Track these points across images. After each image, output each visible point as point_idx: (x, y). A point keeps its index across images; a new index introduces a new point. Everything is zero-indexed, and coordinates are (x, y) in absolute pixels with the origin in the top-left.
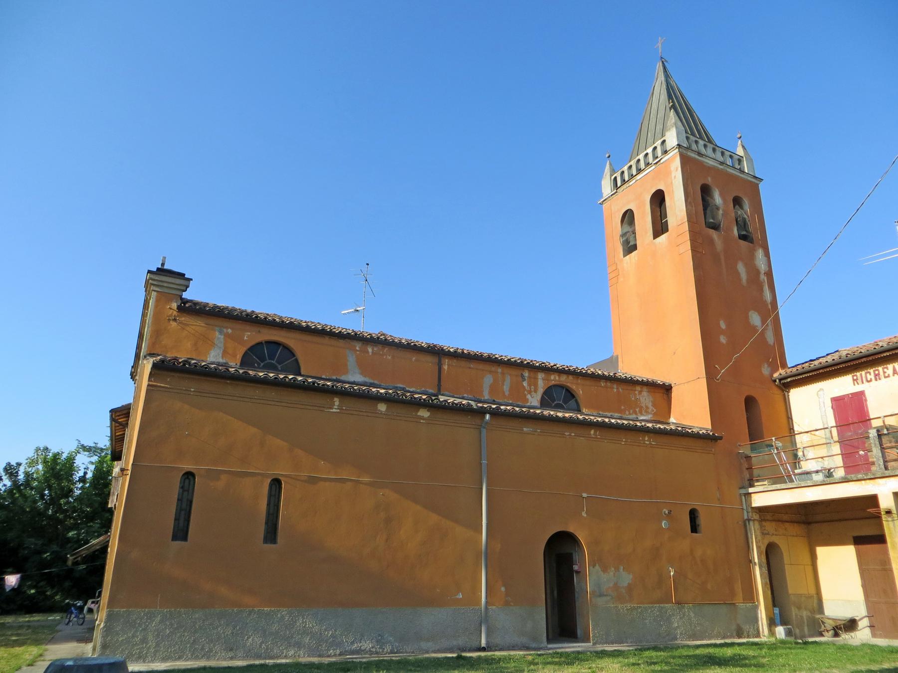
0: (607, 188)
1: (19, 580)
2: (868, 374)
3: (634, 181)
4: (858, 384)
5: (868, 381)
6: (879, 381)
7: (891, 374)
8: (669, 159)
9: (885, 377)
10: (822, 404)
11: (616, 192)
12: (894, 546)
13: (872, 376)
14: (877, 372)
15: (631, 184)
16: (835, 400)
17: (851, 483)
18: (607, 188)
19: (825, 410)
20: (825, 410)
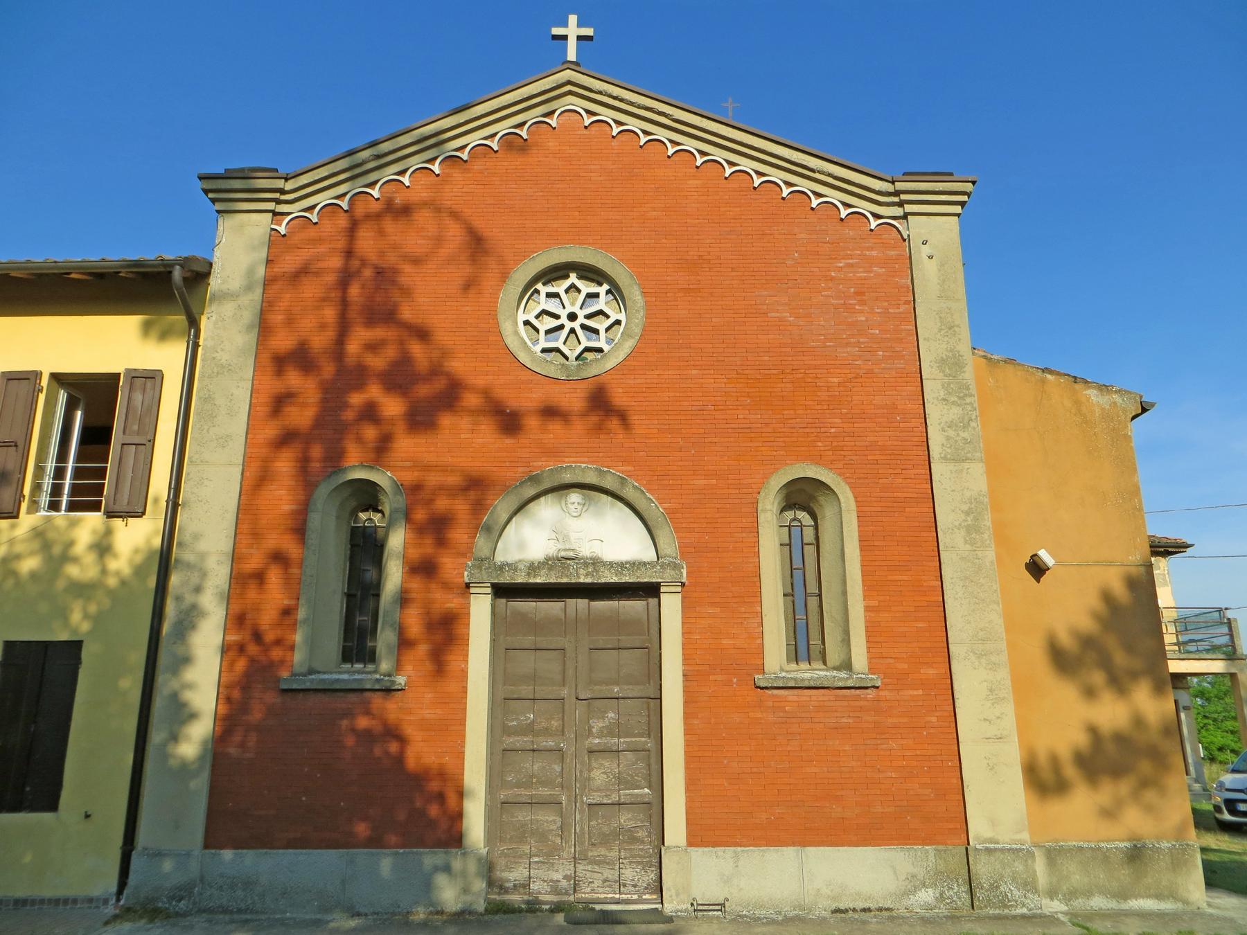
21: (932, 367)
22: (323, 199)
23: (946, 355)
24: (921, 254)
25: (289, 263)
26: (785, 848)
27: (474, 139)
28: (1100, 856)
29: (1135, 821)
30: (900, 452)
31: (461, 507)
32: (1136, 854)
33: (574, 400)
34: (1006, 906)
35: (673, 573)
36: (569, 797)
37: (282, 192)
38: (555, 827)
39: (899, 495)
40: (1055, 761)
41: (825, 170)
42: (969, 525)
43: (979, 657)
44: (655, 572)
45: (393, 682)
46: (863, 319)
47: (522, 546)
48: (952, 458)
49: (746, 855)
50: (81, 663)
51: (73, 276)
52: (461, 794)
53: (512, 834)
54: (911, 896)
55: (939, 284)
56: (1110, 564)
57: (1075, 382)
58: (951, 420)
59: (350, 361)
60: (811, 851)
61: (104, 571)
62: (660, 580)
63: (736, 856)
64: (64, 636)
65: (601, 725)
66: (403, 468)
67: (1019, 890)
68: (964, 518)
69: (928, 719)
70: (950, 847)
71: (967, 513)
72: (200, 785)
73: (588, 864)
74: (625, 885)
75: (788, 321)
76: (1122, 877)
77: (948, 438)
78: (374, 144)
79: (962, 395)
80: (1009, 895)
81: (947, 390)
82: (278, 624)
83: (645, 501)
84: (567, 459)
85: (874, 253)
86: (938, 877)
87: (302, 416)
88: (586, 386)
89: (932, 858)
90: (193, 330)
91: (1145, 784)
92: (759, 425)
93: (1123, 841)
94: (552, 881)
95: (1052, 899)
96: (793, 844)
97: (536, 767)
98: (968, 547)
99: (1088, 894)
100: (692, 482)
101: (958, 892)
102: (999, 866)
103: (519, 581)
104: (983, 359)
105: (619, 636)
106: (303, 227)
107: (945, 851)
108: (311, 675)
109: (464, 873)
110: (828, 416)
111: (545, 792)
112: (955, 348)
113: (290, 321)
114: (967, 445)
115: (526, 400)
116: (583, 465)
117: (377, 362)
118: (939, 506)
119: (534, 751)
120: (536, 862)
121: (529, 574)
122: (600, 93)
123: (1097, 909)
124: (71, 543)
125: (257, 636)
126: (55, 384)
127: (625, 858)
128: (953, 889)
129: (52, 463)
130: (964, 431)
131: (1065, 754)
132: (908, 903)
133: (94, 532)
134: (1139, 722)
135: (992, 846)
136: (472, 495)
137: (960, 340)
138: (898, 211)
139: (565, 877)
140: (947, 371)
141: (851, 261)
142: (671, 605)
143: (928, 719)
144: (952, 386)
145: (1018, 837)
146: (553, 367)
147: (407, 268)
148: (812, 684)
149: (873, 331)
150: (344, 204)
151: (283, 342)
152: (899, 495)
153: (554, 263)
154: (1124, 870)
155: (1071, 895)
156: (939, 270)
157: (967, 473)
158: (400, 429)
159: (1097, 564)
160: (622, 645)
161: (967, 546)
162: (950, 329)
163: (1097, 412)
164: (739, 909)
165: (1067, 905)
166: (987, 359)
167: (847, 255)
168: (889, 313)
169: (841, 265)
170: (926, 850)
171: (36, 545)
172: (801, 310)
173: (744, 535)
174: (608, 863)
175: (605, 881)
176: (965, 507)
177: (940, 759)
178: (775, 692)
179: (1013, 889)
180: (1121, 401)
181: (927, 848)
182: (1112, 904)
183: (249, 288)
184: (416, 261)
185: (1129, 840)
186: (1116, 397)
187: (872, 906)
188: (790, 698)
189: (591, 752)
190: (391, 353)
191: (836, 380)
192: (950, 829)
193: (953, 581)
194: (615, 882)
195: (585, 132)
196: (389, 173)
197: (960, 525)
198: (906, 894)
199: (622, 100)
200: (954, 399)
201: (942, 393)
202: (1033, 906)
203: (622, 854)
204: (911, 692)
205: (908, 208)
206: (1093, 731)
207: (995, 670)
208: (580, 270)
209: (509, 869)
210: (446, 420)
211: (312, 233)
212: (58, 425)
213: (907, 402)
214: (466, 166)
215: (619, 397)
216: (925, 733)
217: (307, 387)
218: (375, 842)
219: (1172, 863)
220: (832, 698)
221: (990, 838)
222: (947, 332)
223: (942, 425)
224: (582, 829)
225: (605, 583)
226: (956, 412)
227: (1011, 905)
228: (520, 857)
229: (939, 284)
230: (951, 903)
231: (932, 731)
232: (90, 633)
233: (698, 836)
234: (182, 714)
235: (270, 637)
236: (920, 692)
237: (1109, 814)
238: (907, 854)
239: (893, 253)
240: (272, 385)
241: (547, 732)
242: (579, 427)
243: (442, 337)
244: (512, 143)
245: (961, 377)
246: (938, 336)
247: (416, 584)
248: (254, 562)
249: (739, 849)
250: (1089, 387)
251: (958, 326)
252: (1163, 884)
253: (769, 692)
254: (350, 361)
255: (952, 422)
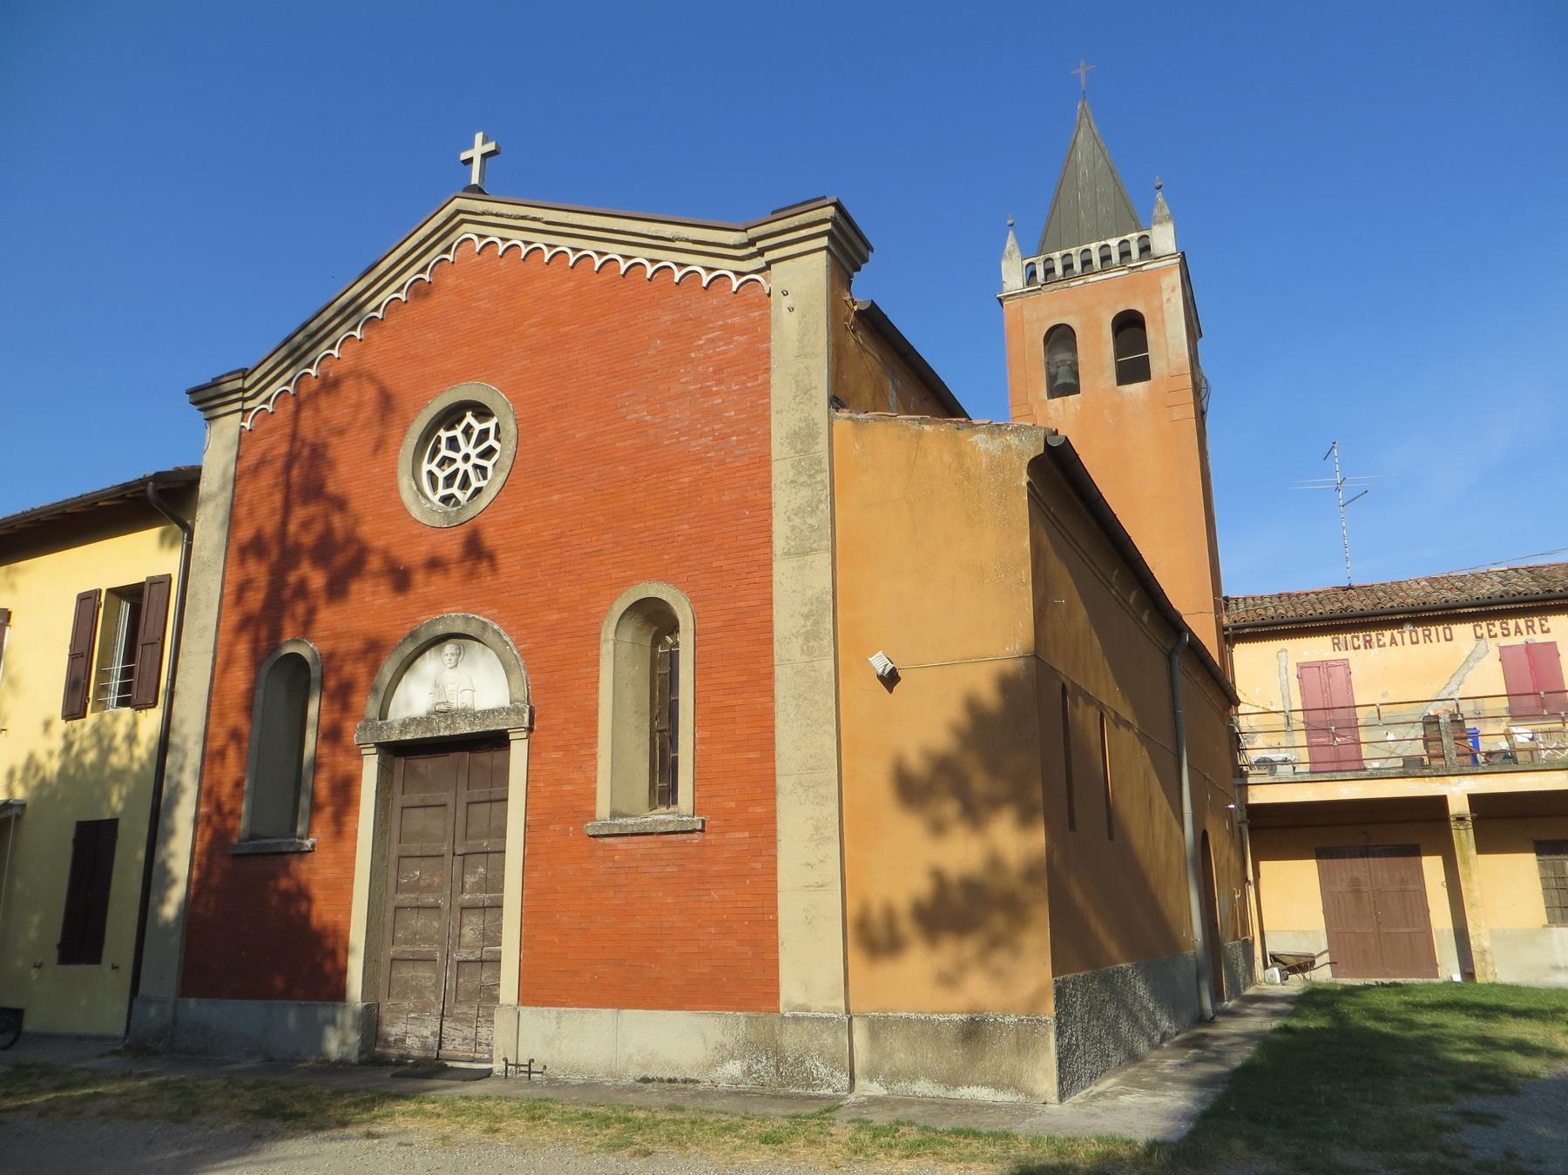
0: (1012, 276)
1: (183, 907)
2: (1355, 639)
3: (1082, 282)
4: (1340, 650)
5: (1355, 648)
6: (1369, 650)
7: (1388, 643)
8: (1157, 268)
9: (1379, 646)
10: (1283, 670)
11: (1040, 289)
12: (1465, 860)
13: (1361, 642)
14: (1368, 638)
15: (1072, 284)
16: (1302, 667)
17: (1408, 779)
18: (1012, 276)
19: (1287, 679)
20: (1287, 679)
21: (783, 445)
22: (275, 389)
23: (799, 427)
24: (780, 305)
25: (251, 459)
26: (602, 1010)
27: (386, 296)
28: (926, 1030)
29: (979, 991)
30: (746, 553)
31: (361, 670)
32: (973, 1031)
33: (452, 547)
34: (809, 1085)
35: (516, 718)
36: (442, 953)
37: (244, 390)
38: (430, 984)
39: (742, 604)
40: (890, 916)
41: (681, 236)
42: (808, 631)
43: (806, 790)
44: (502, 719)
45: (302, 845)
46: (720, 401)
47: (408, 704)
48: (796, 552)
49: (567, 1015)
50: (117, 837)
51: (100, 504)
52: (347, 950)
53: (398, 989)
54: (719, 1069)
55: (798, 340)
56: (980, 660)
57: (958, 429)
58: (798, 505)
59: (290, 541)
60: (627, 1013)
61: (132, 758)
62: (505, 727)
63: (559, 1016)
64: (107, 816)
65: (473, 880)
66: (323, 638)
67: (826, 1068)
68: (803, 623)
69: (754, 865)
70: (762, 1014)
71: (806, 617)
72: (175, 942)
73: (453, 1021)
74: (480, 1044)
75: (646, 421)
76: (954, 1058)
77: (793, 528)
78: (304, 326)
79: (813, 472)
80: (815, 1072)
81: (796, 470)
82: (232, 796)
83: (501, 644)
84: (444, 610)
85: (736, 319)
86: (750, 1048)
87: (255, 600)
88: (463, 530)
89: (742, 1026)
90: (186, 535)
91: (995, 943)
92: (610, 546)
93: (962, 1013)
94: (422, 1037)
95: (871, 1081)
96: (612, 1006)
97: (419, 924)
98: (805, 658)
99: (913, 1077)
100: (546, 618)
101: (764, 1066)
102: (806, 1038)
103: (394, 739)
104: (849, 422)
105: (492, 787)
106: (264, 419)
107: (757, 1018)
108: (254, 840)
109: (343, 1026)
110: (676, 523)
111: (425, 948)
112: (809, 415)
113: (251, 512)
114: (814, 533)
115: (410, 556)
116: (453, 614)
117: (308, 539)
118: (777, 612)
119: (418, 907)
120: (413, 1018)
121: (401, 731)
122: (483, 214)
123: (920, 1095)
124: (113, 737)
125: (219, 808)
126: (115, 598)
127: (482, 1017)
128: (762, 1062)
129: (118, 665)
130: (811, 517)
131: (902, 904)
132: (713, 1075)
133: (127, 725)
134: (995, 863)
135: (800, 1014)
136: (371, 656)
137: (816, 404)
138: (759, 263)
139: (433, 1034)
140: (799, 446)
141: (711, 336)
142: (518, 750)
143: (754, 865)
144: (803, 463)
145: (833, 1004)
146: (438, 517)
147: (334, 441)
148: (636, 830)
149: (727, 414)
150: (290, 389)
151: (245, 533)
152: (742, 604)
153: (447, 404)
154: (958, 1049)
155: (894, 1076)
156: (800, 323)
157: (811, 568)
158: (321, 602)
159: (966, 661)
160: (493, 797)
161: (804, 657)
162: (806, 393)
163: (985, 460)
164: (557, 1072)
165: (887, 1089)
166: (853, 420)
167: (709, 328)
168: (746, 387)
169: (701, 342)
170: (738, 1016)
171: (94, 740)
172: (658, 406)
173: (589, 669)
174: (468, 1021)
175: (464, 1039)
176: (805, 610)
177: (761, 912)
178: (607, 840)
179: (819, 1065)
180: (1017, 443)
181: (738, 1014)
182: (940, 1091)
183: (223, 488)
184: (341, 432)
185: (969, 1012)
186: (1012, 439)
187: (679, 1077)
188: (620, 847)
189: (463, 908)
190: (318, 528)
191: (687, 480)
192: (767, 993)
193: (786, 700)
194: (473, 1040)
195: (478, 258)
196: (322, 350)
197: (798, 632)
198: (713, 1065)
199: (501, 216)
200: (803, 478)
201: (791, 474)
202: (839, 1086)
203: (480, 1012)
204: (737, 835)
205: (769, 256)
206: (938, 876)
207: (823, 805)
208: (475, 407)
209: (392, 1024)
210: (355, 587)
211: (269, 424)
212: (122, 637)
213: (758, 492)
214: (383, 324)
215: (490, 538)
216: (748, 882)
217: (258, 571)
218: (287, 995)
219: (1017, 1043)
220: (659, 845)
221: (801, 1006)
222: (802, 398)
223: (788, 514)
224: (451, 986)
225: (451, 736)
226: (805, 494)
227: (815, 1084)
228: (401, 1012)
229: (798, 340)
230: (758, 1078)
231: (756, 879)
232: (123, 811)
233: (531, 994)
234: (168, 880)
235: (227, 808)
236: (747, 834)
237: (947, 980)
238: (718, 1019)
239: (756, 313)
240: (235, 576)
241: (429, 889)
242: (456, 574)
243: (356, 505)
244: (419, 291)
245: (813, 451)
246: (793, 406)
247: (325, 750)
248: (217, 743)
249: (563, 1009)
250: (976, 432)
251: (816, 388)
252: (1003, 1068)
253: (601, 840)
254: (290, 541)
255: (799, 507)
